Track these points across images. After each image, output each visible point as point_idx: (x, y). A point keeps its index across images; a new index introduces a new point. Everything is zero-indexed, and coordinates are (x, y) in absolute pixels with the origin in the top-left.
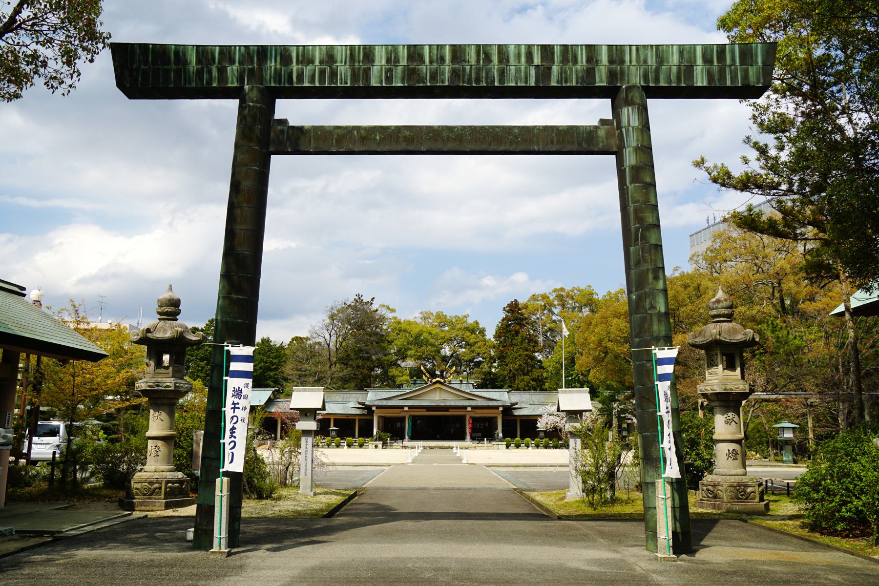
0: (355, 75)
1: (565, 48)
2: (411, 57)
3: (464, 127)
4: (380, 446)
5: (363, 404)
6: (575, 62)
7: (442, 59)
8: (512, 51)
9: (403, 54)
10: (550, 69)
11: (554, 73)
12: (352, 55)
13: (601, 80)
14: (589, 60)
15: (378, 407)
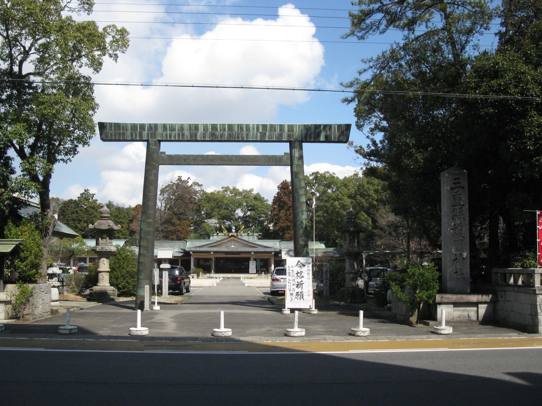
0: (191, 136)
1: (271, 125)
2: (212, 128)
3: (233, 156)
4: (196, 277)
5: (184, 250)
6: (275, 131)
7: (224, 129)
8: (251, 126)
9: (210, 127)
10: (265, 134)
11: (266, 134)
12: (190, 127)
13: (285, 138)
14: (281, 130)
15: (194, 252)
